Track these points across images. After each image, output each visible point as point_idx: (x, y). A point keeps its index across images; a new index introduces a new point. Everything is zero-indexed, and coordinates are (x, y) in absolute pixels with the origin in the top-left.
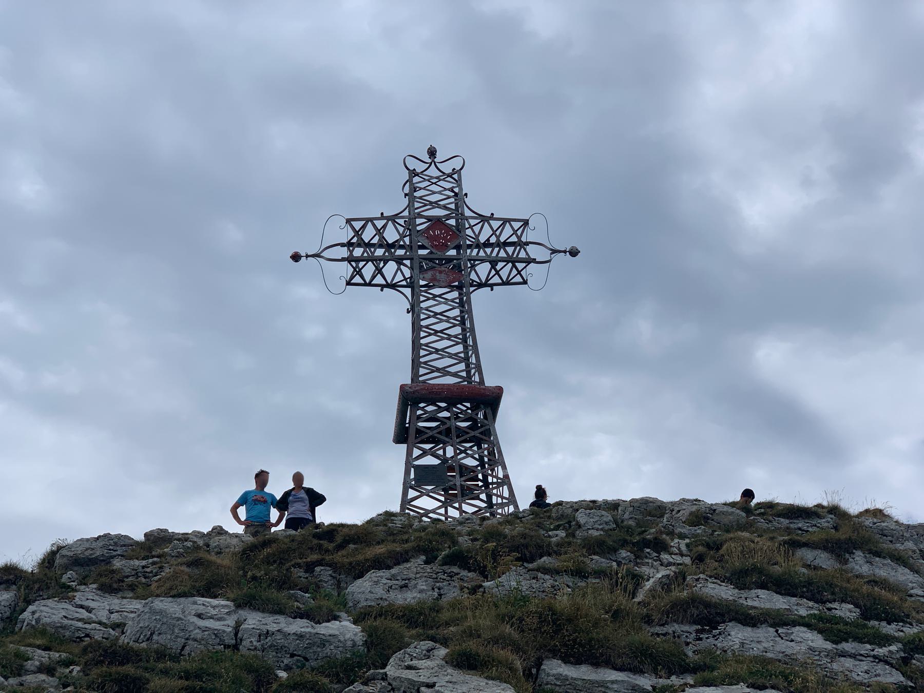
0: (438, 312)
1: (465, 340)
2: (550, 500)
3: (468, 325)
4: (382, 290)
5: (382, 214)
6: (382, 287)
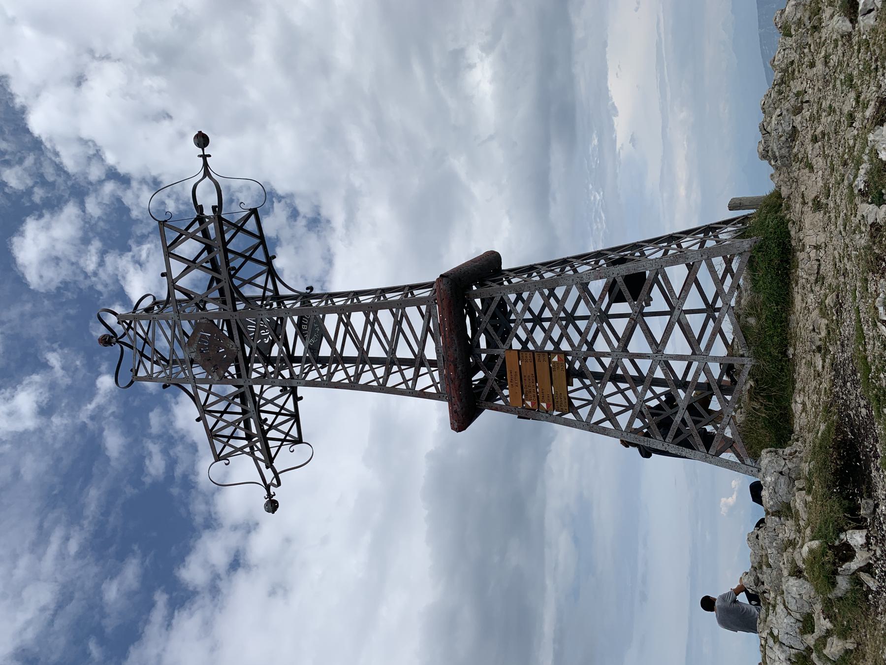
4: (301, 398)
5: (198, 420)
6: (166, 274)
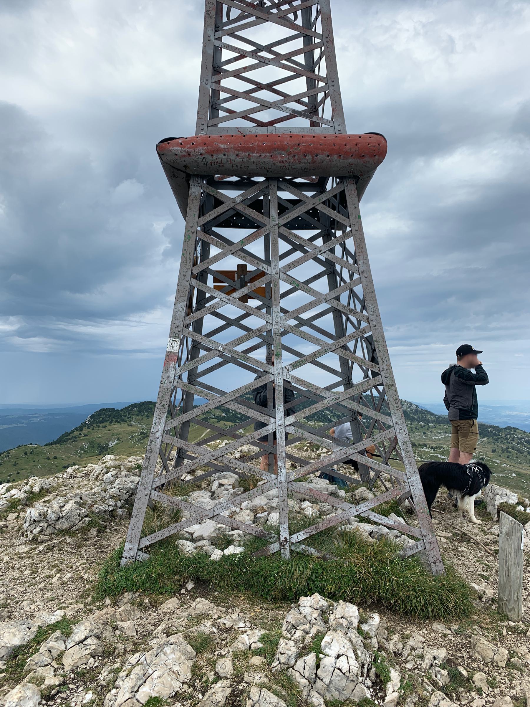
0: (264, 82)
1: (310, 67)
2: (478, 388)
3: (322, 70)
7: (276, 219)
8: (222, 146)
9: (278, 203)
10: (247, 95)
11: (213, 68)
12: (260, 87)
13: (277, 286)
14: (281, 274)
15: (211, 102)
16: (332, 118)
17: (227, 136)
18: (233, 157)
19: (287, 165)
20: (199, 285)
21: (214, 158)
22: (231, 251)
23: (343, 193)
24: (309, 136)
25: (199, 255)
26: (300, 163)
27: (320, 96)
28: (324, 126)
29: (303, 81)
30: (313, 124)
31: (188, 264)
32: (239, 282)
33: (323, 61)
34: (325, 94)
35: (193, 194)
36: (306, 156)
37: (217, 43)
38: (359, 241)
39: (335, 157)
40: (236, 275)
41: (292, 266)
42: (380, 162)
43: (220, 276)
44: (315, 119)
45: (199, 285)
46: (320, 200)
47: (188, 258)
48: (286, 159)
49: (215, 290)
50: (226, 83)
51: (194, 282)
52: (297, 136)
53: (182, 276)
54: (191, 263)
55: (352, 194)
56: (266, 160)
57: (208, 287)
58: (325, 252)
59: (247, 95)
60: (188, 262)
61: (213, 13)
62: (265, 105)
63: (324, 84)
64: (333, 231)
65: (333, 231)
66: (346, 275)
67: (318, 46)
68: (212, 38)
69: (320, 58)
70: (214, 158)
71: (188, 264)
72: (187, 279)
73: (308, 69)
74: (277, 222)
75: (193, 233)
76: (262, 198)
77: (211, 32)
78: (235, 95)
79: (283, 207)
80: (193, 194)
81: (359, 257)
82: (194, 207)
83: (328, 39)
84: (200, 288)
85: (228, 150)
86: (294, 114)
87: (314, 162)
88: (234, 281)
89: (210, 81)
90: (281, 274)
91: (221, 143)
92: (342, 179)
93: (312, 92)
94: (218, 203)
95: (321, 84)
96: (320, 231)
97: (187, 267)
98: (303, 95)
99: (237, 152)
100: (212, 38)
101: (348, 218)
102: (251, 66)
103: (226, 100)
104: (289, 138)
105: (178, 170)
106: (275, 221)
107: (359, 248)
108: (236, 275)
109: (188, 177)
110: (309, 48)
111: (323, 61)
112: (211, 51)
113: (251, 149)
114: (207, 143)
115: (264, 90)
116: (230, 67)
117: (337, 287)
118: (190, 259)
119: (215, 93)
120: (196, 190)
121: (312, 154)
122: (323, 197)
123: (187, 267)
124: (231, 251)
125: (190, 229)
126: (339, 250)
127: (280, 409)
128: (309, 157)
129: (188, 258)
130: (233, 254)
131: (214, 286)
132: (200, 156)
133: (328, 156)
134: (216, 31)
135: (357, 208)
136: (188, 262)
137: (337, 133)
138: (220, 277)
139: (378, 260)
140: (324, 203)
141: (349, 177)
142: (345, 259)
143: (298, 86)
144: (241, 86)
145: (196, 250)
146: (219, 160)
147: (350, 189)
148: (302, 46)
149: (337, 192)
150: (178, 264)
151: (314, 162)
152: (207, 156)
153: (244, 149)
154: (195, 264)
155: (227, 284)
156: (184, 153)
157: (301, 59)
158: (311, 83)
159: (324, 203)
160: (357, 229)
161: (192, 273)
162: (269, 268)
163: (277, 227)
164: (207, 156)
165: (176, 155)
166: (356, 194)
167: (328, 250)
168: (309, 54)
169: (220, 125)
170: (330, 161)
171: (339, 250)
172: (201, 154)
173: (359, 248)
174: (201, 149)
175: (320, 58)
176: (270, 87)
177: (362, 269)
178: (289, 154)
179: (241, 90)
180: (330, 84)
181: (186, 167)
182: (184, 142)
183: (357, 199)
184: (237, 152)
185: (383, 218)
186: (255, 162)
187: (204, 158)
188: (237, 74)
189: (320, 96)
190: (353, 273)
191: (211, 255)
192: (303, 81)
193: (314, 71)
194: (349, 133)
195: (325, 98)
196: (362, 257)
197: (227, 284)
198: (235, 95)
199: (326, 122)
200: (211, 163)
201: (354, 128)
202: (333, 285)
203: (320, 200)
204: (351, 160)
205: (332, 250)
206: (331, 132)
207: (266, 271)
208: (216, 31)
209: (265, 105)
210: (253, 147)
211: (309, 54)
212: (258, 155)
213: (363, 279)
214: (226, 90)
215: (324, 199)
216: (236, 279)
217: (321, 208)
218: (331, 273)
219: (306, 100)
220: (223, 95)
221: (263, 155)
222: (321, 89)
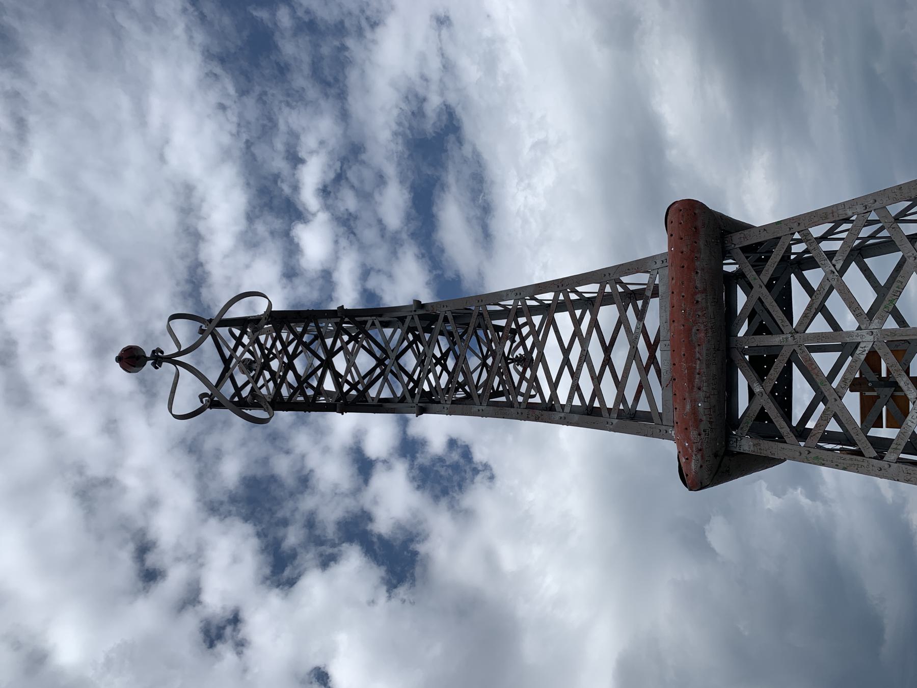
0: (561, 357)
3: (548, 297)
7: (784, 336)
8: (688, 407)
9: (755, 334)
10: (575, 375)
11: (589, 415)
12: (566, 362)
13: (892, 332)
14: (872, 327)
15: (627, 419)
16: (647, 272)
17: (675, 401)
18: (701, 394)
19: (709, 325)
20: (896, 449)
21: (704, 418)
22: (836, 400)
23: (746, 250)
24: (672, 299)
25: (839, 447)
26: (707, 308)
27: (573, 296)
28: (657, 282)
29: (558, 317)
30: (655, 294)
31: (860, 463)
32: (881, 389)
33: (539, 297)
34: (571, 292)
35: (752, 448)
36: (697, 302)
37: (567, 410)
38: (816, 219)
39: (698, 263)
40: (867, 394)
41: (857, 312)
42: (702, 206)
43: (870, 417)
44: (649, 293)
45: (896, 449)
46: (755, 279)
47: (850, 462)
48: (702, 327)
49: (904, 426)
50: (563, 398)
51: (890, 456)
52: (672, 314)
53: (881, 473)
54: (859, 458)
55: (745, 238)
56: (704, 352)
57: (898, 436)
58: (834, 266)
59: (575, 375)
60: (856, 463)
61: (537, 412)
62: (585, 357)
63: (608, 286)
64: (792, 257)
65: (792, 257)
66: (865, 232)
67: (567, 296)
68: (562, 415)
69: (536, 300)
70: (704, 418)
71: (860, 463)
72: (887, 466)
73: (548, 311)
74: (789, 336)
75: (809, 452)
76: (747, 357)
77: (557, 416)
78: (576, 388)
79: (759, 329)
80: (752, 448)
81: (835, 216)
82: (769, 448)
83: (520, 293)
84: (901, 447)
85: (694, 402)
86: (594, 324)
87: (704, 291)
88: (878, 397)
89: (609, 420)
90: (872, 327)
91: (684, 408)
92: (725, 253)
93: (617, 298)
94: (762, 415)
95: (561, 297)
96: (792, 275)
97: (865, 464)
98: (573, 316)
99: (695, 389)
100: (562, 415)
101: (780, 238)
102: (590, 371)
103: (581, 397)
104: (675, 324)
105: (720, 466)
106: (787, 338)
107: (826, 218)
108: (867, 394)
109: (729, 453)
110: (569, 306)
111: (539, 297)
112: (576, 417)
113: (691, 370)
114: (684, 427)
115: (611, 356)
116: (547, 393)
117: (812, 257)
118: (851, 459)
119: (574, 410)
120: (747, 445)
121: (695, 294)
122: (751, 274)
123: (865, 464)
124: (836, 400)
125: (803, 456)
126: (826, 246)
127: (775, 340)
128: (699, 297)
129: (850, 462)
130: (841, 398)
131: (887, 427)
132: (702, 436)
133: (697, 273)
134: (555, 410)
135: (765, 228)
136: (856, 463)
137: (665, 264)
138: (872, 417)
139: (842, 191)
140: (759, 272)
141: (723, 243)
142: (844, 235)
143: (563, 319)
144: (566, 381)
145: (832, 450)
146: (706, 412)
147: (739, 240)
148: (566, 314)
149: (742, 256)
150: (826, 472)
151: (704, 291)
152: (702, 426)
153: (691, 381)
154: (859, 453)
155: (884, 409)
156: (699, 456)
157: (537, 320)
158: (561, 307)
159: (759, 272)
160: (796, 224)
161: (874, 458)
162: (862, 345)
163: (797, 336)
164: (702, 426)
165: (701, 466)
166: (746, 232)
167: (831, 261)
168: (533, 311)
169: (660, 411)
170: (703, 270)
171: (826, 246)
172: (700, 435)
173: (826, 218)
174: (693, 434)
175: (536, 300)
176: (566, 352)
177: (860, 209)
178: (695, 323)
179: (570, 381)
180: (607, 277)
181: (716, 455)
182: (683, 454)
183: (752, 230)
184: (695, 389)
185: (757, 198)
186: (708, 366)
187: (704, 431)
188: (554, 386)
189: (573, 296)
190: (793, 240)
191: (839, 429)
192: (558, 317)
193: (549, 305)
194: (666, 250)
195: (576, 292)
196: (841, 212)
197: (884, 409)
198: (576, 388)
199: (652, 279)
200: (711, 423)
201: (657, 243)
202: (812, 264)
203: (755, 279)
204: (701, 243)
205: (831, 255)
206: (666, 271)
207: (867, 349)
208: (555, 410)
209: (585, 357)
210: (689, 368)
211: (533, 311)
212: (698, 362)
213: (877, 205)
214: (570, 398)
215: (754, 273)
216: (875, 394)
217: (766, 277)
218: (859, 253)
219: (578, 313)
220: (576, 402)
221: (698, 355)
222: (613, 286)
